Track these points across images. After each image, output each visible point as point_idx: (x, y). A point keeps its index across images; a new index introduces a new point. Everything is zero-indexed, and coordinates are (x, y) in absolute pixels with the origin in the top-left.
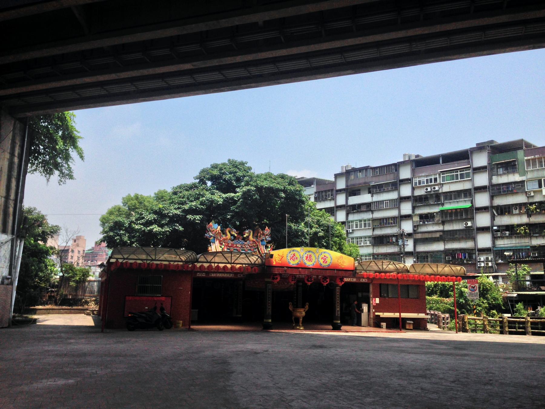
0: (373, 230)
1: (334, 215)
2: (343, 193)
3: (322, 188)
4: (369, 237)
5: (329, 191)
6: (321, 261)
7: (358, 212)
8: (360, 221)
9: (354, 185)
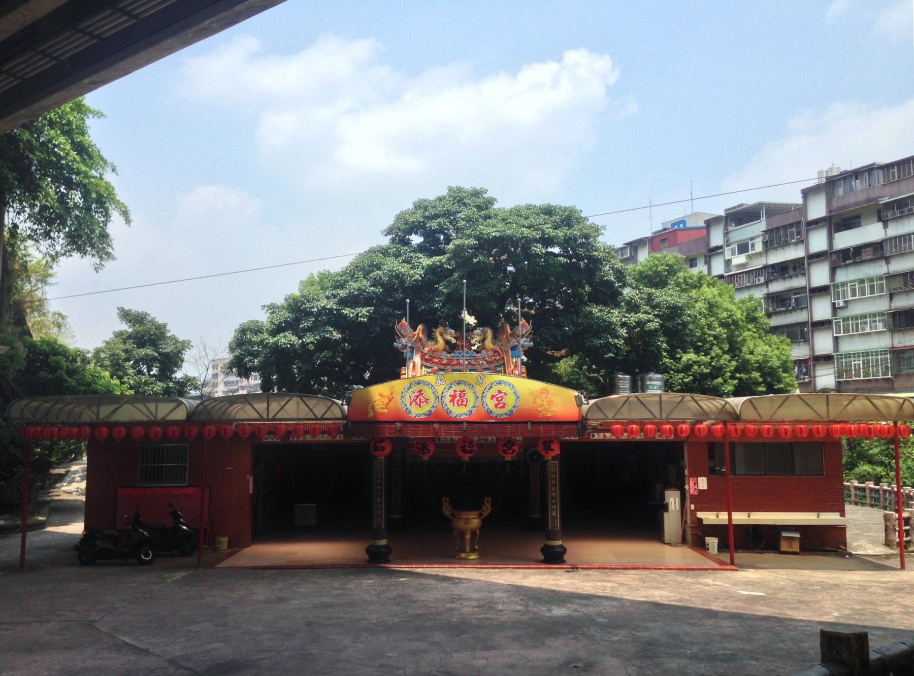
0: (891, 299)
1: (804, 274)
2: (822, 227)
3: (779, 221)
4: (882, 314)
5: (791, 225)
6: (491, 404)
7: (856, 263)
8: (862, 281)
9: (844, 207)
